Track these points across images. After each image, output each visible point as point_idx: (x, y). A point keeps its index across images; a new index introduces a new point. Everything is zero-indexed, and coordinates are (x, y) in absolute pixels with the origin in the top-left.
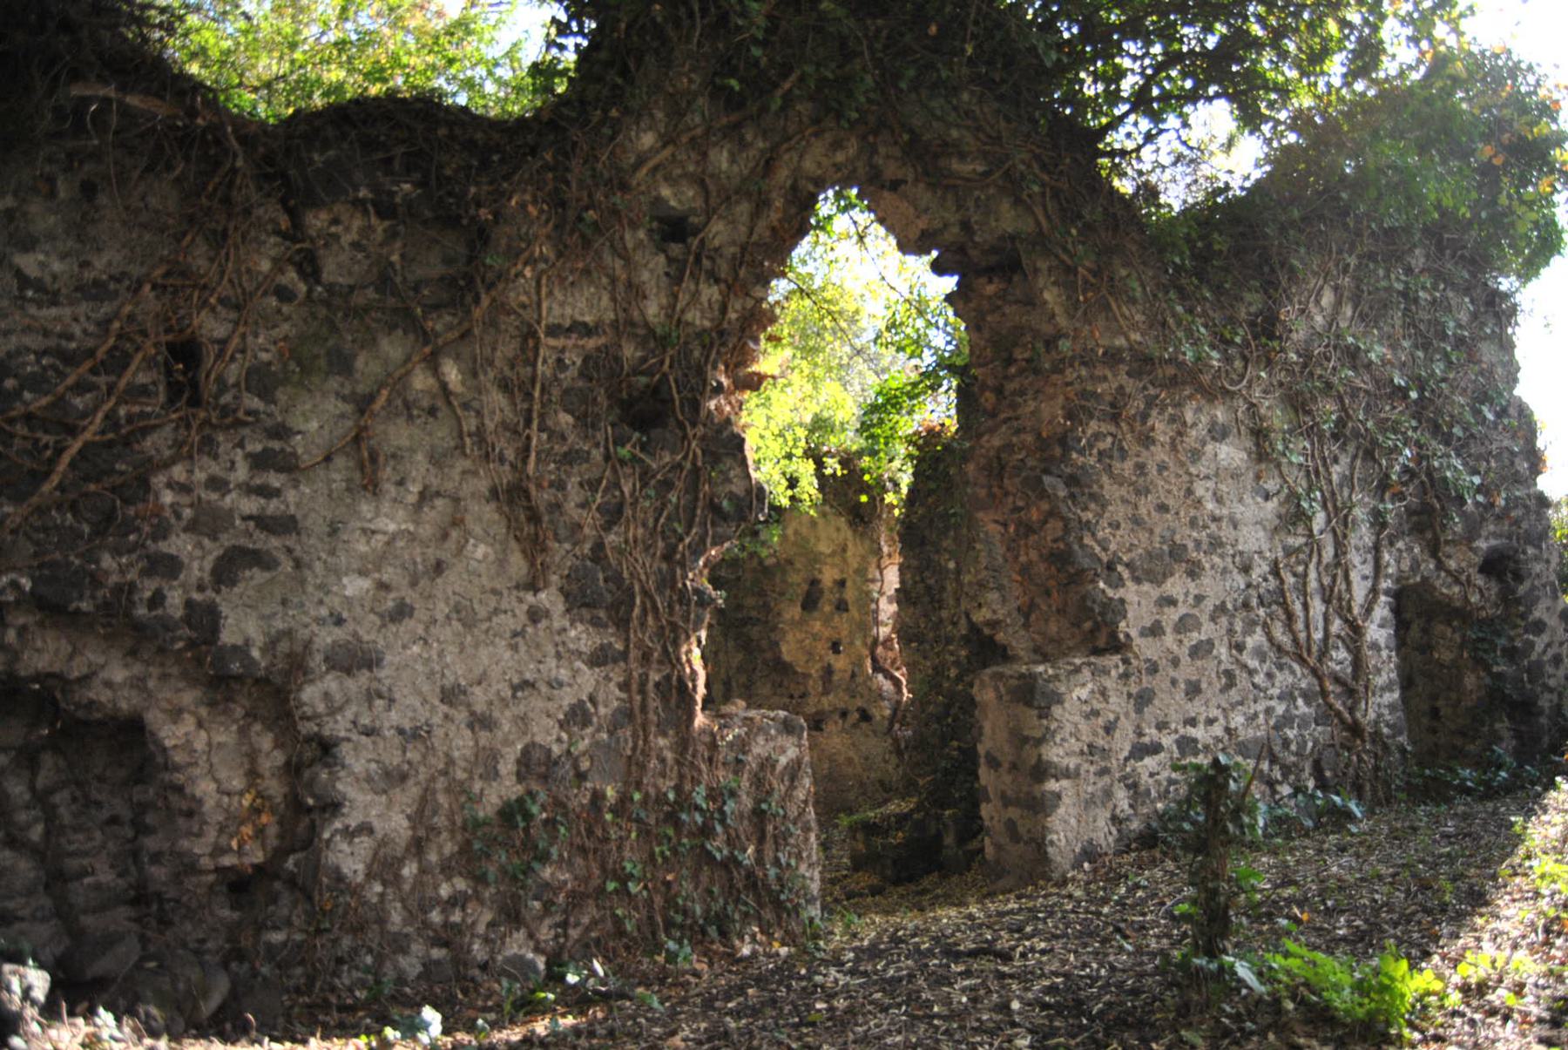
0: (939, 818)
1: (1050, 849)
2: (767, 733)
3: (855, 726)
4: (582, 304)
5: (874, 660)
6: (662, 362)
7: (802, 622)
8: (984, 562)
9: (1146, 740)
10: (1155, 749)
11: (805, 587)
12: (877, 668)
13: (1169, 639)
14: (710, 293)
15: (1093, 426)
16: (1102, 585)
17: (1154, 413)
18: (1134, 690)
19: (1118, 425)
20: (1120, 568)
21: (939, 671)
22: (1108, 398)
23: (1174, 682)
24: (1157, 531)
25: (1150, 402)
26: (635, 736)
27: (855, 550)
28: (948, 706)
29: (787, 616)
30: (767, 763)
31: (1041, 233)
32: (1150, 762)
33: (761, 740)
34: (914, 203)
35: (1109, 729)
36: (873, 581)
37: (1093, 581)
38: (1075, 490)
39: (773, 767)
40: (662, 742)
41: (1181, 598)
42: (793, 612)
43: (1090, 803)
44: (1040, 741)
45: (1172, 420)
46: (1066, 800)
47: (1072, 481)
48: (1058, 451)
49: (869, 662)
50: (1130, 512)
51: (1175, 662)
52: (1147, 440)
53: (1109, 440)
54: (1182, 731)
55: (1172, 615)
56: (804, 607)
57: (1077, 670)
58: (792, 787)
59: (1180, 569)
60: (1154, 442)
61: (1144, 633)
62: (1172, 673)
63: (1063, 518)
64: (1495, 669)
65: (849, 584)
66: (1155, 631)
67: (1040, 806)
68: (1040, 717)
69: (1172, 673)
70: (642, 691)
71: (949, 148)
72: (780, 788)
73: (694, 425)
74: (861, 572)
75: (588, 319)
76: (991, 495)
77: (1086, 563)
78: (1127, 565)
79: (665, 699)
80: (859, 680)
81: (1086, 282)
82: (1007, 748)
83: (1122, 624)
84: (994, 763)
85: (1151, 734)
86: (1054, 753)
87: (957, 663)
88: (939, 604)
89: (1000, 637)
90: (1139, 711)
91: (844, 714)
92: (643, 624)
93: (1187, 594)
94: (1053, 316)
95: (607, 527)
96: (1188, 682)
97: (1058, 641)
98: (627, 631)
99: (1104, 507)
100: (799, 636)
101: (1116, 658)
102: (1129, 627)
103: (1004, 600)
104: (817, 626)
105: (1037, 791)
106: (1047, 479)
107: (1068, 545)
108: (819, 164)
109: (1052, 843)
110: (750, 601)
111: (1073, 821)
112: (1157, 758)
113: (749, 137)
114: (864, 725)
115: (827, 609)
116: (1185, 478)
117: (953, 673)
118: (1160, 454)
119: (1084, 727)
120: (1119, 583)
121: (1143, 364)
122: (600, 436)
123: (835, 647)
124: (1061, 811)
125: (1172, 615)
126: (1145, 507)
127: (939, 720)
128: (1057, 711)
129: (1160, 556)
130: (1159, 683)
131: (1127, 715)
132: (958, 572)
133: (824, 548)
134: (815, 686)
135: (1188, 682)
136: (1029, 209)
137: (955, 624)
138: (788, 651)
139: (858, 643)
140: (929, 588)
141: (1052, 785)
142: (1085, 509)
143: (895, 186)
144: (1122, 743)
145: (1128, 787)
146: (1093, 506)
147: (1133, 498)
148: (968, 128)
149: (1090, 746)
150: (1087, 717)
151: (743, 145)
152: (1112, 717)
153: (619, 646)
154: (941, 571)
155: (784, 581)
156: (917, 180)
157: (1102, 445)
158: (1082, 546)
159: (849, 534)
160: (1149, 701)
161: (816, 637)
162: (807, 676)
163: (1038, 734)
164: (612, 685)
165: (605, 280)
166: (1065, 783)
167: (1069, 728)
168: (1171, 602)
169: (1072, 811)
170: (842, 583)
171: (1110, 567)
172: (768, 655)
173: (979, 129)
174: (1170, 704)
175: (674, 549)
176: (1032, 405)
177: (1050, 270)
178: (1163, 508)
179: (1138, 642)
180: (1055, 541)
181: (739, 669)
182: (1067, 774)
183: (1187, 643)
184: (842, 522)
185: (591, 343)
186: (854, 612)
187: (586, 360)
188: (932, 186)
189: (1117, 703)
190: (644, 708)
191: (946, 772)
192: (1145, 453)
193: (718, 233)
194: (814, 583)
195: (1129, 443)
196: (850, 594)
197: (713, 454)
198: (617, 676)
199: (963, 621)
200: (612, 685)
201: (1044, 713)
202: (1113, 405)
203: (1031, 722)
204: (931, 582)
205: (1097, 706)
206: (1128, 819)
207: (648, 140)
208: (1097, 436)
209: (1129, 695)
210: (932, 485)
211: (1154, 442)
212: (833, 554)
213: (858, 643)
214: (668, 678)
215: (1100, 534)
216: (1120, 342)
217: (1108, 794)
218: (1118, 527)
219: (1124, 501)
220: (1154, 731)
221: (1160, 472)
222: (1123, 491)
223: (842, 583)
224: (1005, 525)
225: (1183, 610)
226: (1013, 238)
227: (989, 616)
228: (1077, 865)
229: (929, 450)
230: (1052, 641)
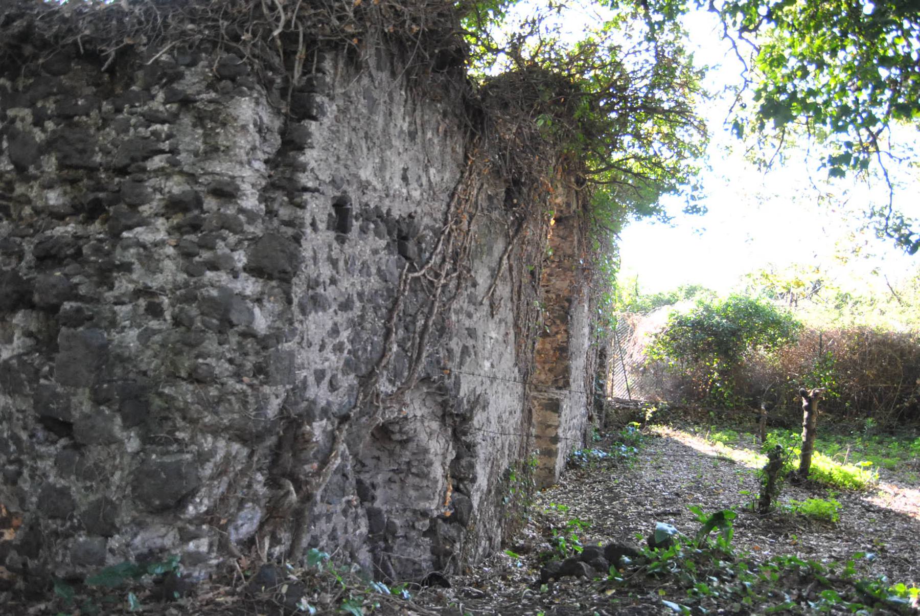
44: (557, 427)
105: (553, 447)
163: (556, 424)
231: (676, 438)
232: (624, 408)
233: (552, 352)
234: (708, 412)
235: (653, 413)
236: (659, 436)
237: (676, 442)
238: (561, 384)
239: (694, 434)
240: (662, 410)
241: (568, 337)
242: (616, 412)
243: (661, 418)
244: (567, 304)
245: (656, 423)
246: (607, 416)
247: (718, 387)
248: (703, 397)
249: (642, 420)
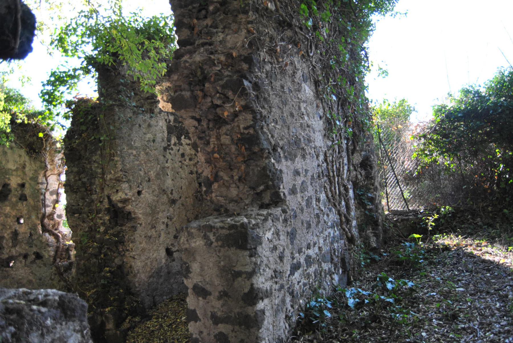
0: (102, 314)
2: (42, 326)
3: (33, 262)
5: (43, 226)
8: (120, 166)
12: (45, 229)
21: (93, 230)
27: (30, 168)
28: (100, 248)
36: (42, 183)
44: (251, 274)
46: (267, 314)
49: (40, 227)
64: (368, 207)
65: (27, 185)
68: (251, 256)
74: (35, 179)
76: (195, 98)
78: (282, 148)
80: (35, 237)
82: (217, 282)
84: (201, 292)
86: (262, 282)
87: (103, 224)
88: (89, 191)
89: (129, 208)
91: (25, 256)
97: (236, 201)
103: (131, 187)
105: (250, 311)
107: (255, 131)
114: (38, 261)
115: (14, 199)
117: (102, 229)
127: (96, 256)
132: (103, 174)
133: (11, 166)
137: (101, 202)
139: (34, 217)
140: (84, 183)
149: (275, 271)
154: (93, 176)
159: (27, 158)
161: (6, 216)
163: (249, 269)
170: (23, 186)
171: (275, 149)
180: (246, 128)
184: (23, 152)
186: (30, 200)
191: (104, 286)
196: (27, 191)
199: (106, 200)
201: (253, 254)
203: (242, 260)
204: (85, 180)
209: (288, 233)
210: (84, 128)
212: (17, 170)
213: (34, 217)
223: (23, 186)
224: (199, 121)
227: (123, 196)
229: (80, 110)
230: (232, 201)
231: (469, 249)
232: (402, 220)
233: (233, 148)
234: (501, 210)
235: (435, 221)
236: (447, 248)
237: (471, 255)
238: (267, 199)
239: (492, 241)
240: (445, 215)
241: (255, 118)
242: (395, 226)
243: (445, 226)
244: (245, 66)
245: (441, 232)
246: (385, 231)
247: (508, 180)
248: (491, 194)
249: (424, 231)
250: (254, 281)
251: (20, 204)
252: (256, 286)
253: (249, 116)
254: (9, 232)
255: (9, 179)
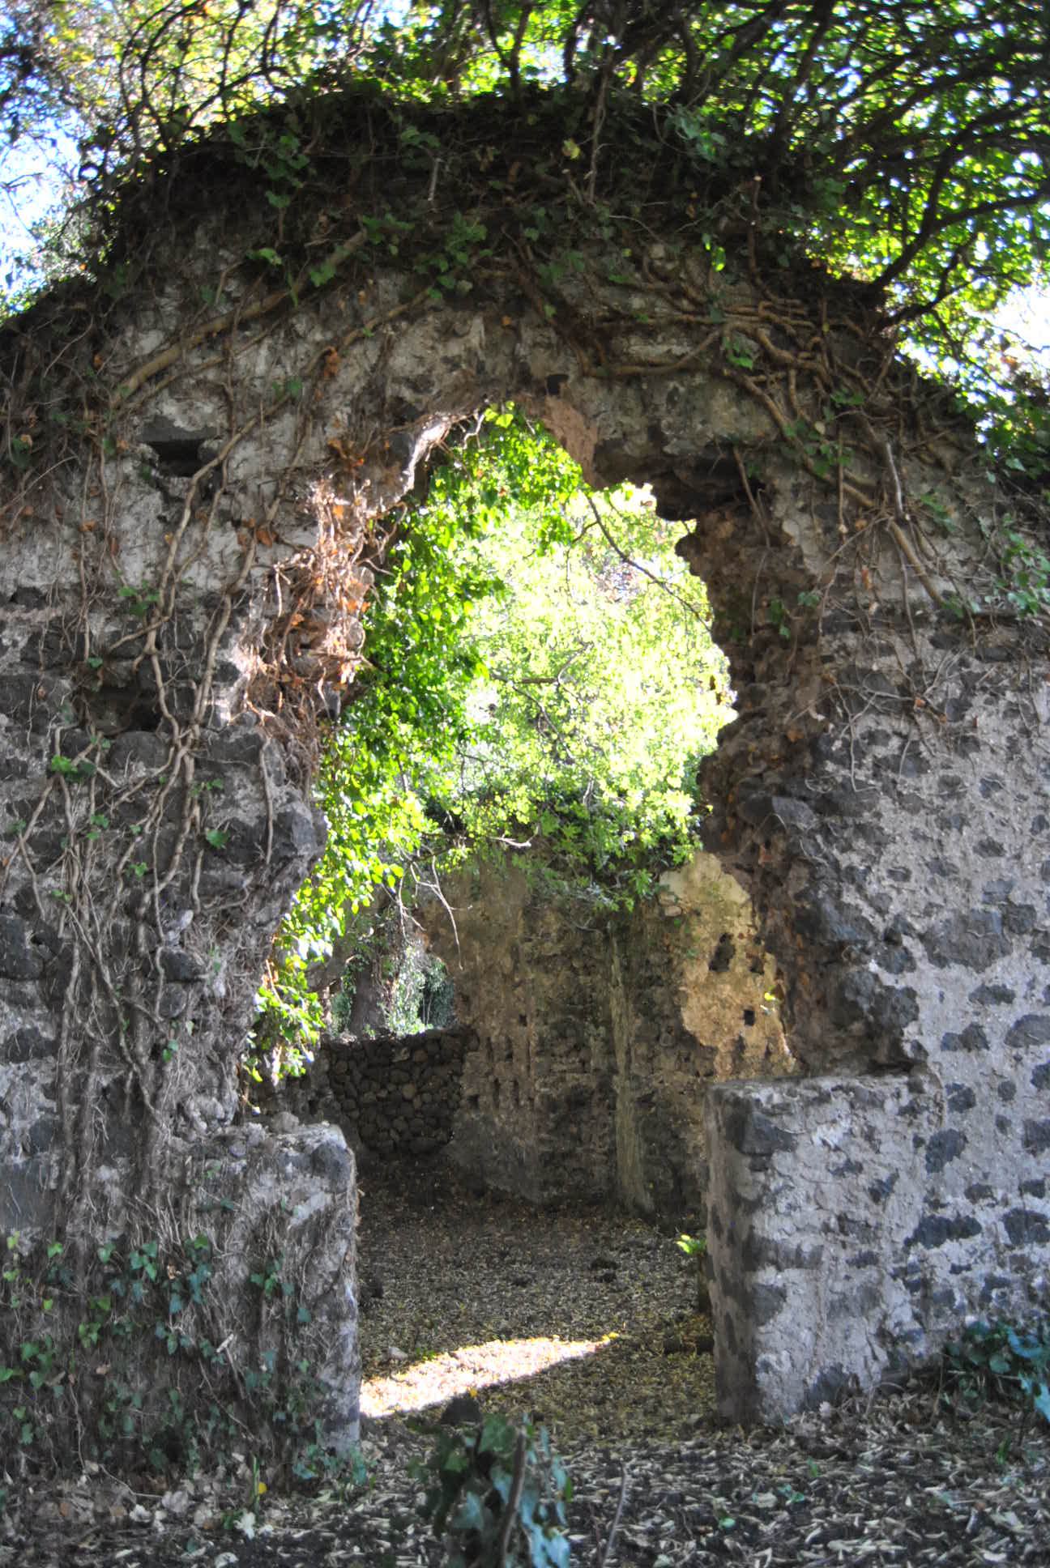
1: (762, 1377)
2: (280, 1170)
4: (32, 563)
6: (143, 638)
7: (708, 985)
9: (948, 1214)
10: (965, 1228)
11: (715, 944)
13: (997, 1056)
14: (224, 542)
15: (864, 723)
16: (873, 966)
17: (979, 700)
18: (927, 1133)
19: (911, 720)
20: (907, 941)
22: (897, 680)
23: (1002, 1124)
24: (979, 884)
25: (969, 685)
26: (62, 1162)
29: (690, 977)
30: (276, 1215)
31: (782, 438)
32: (953, 1250)
33: (267, 1179)
34: (580, 408)
35: (879, 1193)
37: (858, 961)
38: (831, 820)
39: (282, 1222)
40: (105, 1173)
41: (1021, 991)
42: (699, 971)
43: (839, 1307)
44: (754, 1206)
45: (1013, 711)
46: (791, 1297)
47: (826, 805)
48: (808, 760)
50: (929, 853)
51: (1007, 1092)
52: (965, 743)
53: (895, 742)
54: (1016, 1202)
55: (1002, 1018)
56: (714, 967)
57: (823, 1099)
58: (315, 1253)
59: (1021, 945)
60: (977, 745)
61: (947, 1044)
62: (999, 1109)
63: (807, 863)
66: (972, 1040)
67: (758, 1307)
68: (754, 1169)
69: (999, 1109)
70: (77, 1098)
71: (621, 322)
72: (294, 1253)
73: (185, 724)
75: (38, 583)
77: (845, 932)
79: (114, 1110)
80: (774, 1058)
81: (856, 503)
83: (910, 1031)
85: (956, 1204)
86: (772, 1227)
90: (934, 1166)
92: (84, 1004)
93: (1031, 985)
94: (800, 558)
95: (40, 869)
96: (1030, 1125)
98: (60, 1013)
99: (880, 845)
100: (704, 1001)
101: (899, 1082)
102: (921, 1034)
104: (727, 990)
106: (779, 803)
107: (817, 904)
108: (421, 360)
109: (767, 1366)
110: (654, 958)
111: (805, 1336)
112: (967, 1243)
113: (301, 327)
116: (1035, 801)
118: (984, 763)
119: (830, 1185)
120: (907, 963)
121: (956, 628)
122: (44, 742)
123: (749, 1017)
124: (784, 1318)
125: (1002, 1018)
126: (958, 847)
128: (782, 1160)
129: (983, 922)
130: (975, 1124)
131: (911, 1172)
134: (722, 1063)
135: (1030, 1125)
136: (761, 403)
138: (691, 1019)
141: (768, 1276)
142: (847, 848)
143: (553, 385)
144: (902, 1216)
145: (912, 1287)
146: (860, 844)
147: (935, 833)
148: (659, 293)
149: (842, 1219)
150: (839, 1172)
151: (293, 338)
152: (884, 1175)
153: (48, 1034)
155: (688, 936)
156: (584, 375)
157: (880, 751)
158: (841, 907)
160: (956, 1152)
161: (724, 1004)
162: (713, 1050)
164: (34, 1089)
165: (67, 532)
166: (793, 1274)
167: (802, 1189)
168: (1003, 996)
169: (802, 1317)
171: (891, 938)
172: (672, 1023)
173: (679, 294)
174: (998, 1159)
175: (136, 900)
176: (783, 694)
177: (796, 490)
178: (990, 848)
179: (937, 1057)
181: (639, 1038)
182: (797, 1260)
183: (1030, 1062)
185: (41, 617)
187: (34, 639)
188: (607, 381)
189: (895, 1153)
190: (77, 1127)
192: (958, 762)
193: (245, 461)
194: (725, 938)
195: (932, 747)
197: (212, 765)
198: (43, 1076)
200: (34, 1089)
201: (761, 1163)
202: (904, 690)
205: (856, 1155)
206: (909, 1337)
207: (150, 341)
208: (872, 737)
209: (918, 1142)
211: (977, 745)
214: (120, 1082)
215: (872, 889)
216: (915, 594)
217: (872, 1296)
218: (906, 876)
219: (918, 836)
220: (962, 1200)
221: (986, 793)
222: (918, 822)
225: (1021, 1008)
226: (728, 445)
228: (809, 1404)
250: (756, 1222)
251: (749, 980)
252: (758, 1232)
253: (804, 872)
254: (727, 1039)
255: (732, 925)
